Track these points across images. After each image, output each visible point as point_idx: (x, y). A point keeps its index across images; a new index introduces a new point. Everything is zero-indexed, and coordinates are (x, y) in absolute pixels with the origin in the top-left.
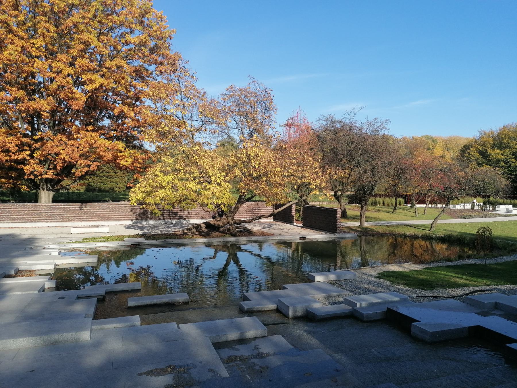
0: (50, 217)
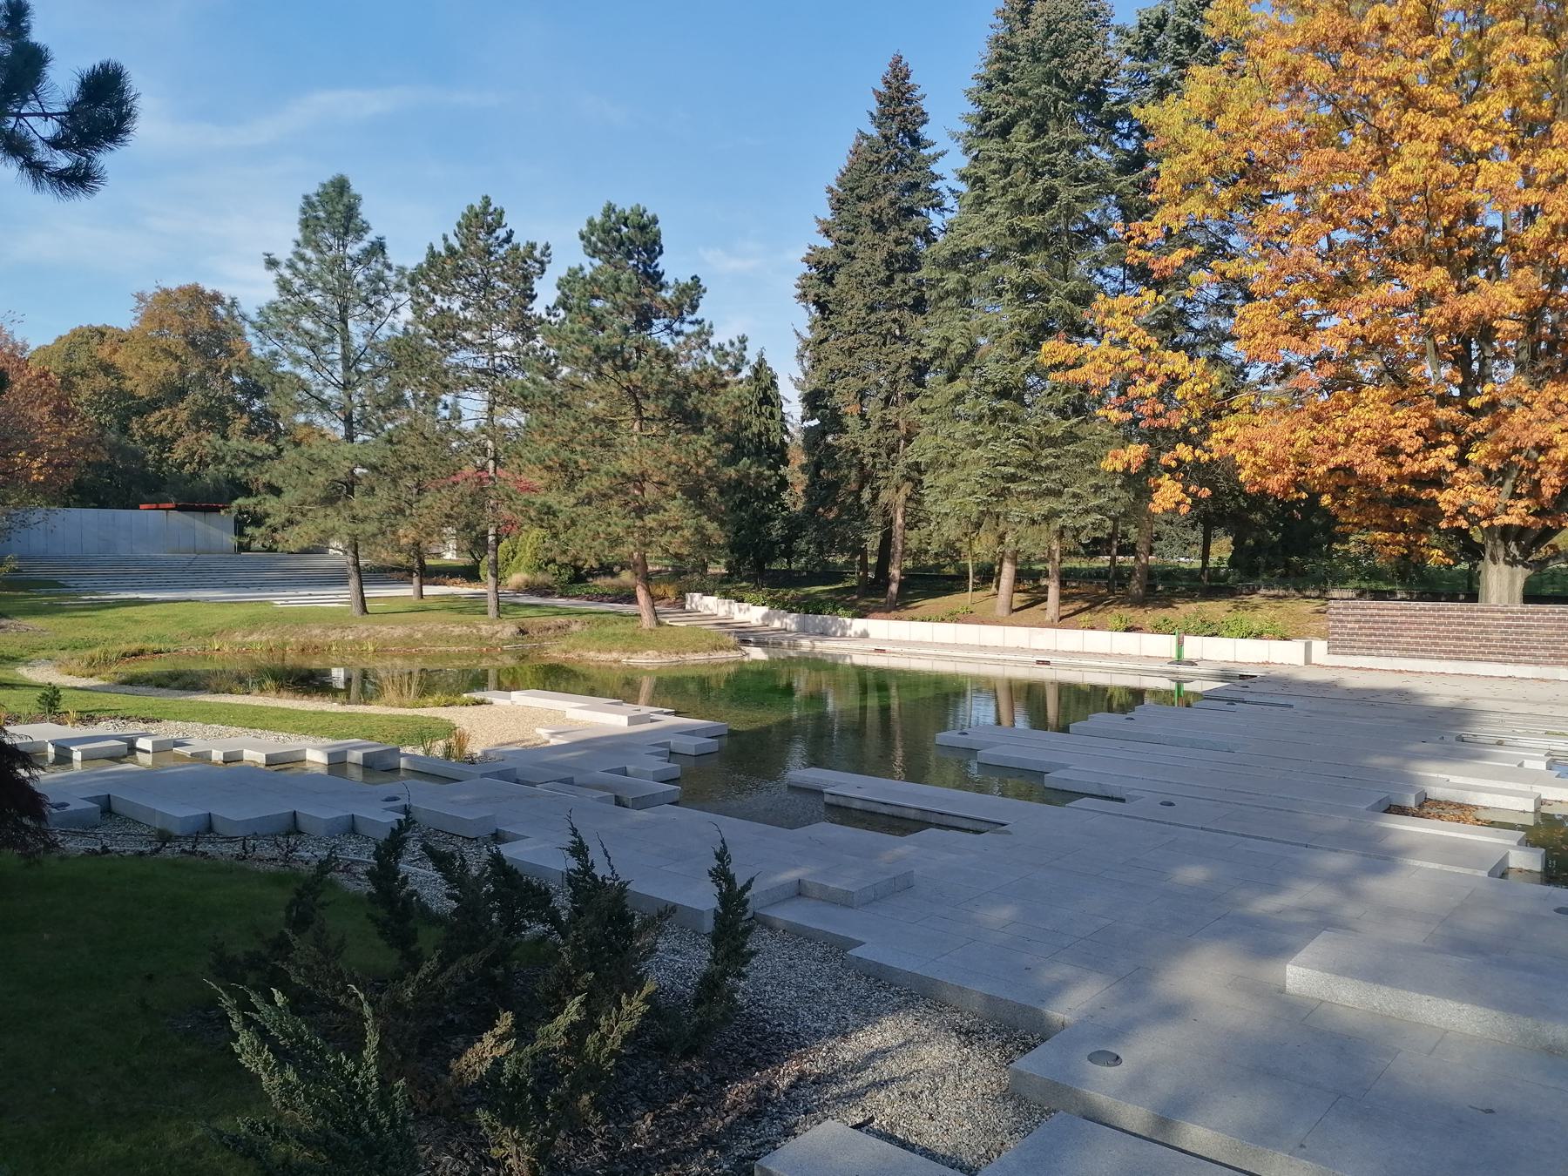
0: (1515, 648)
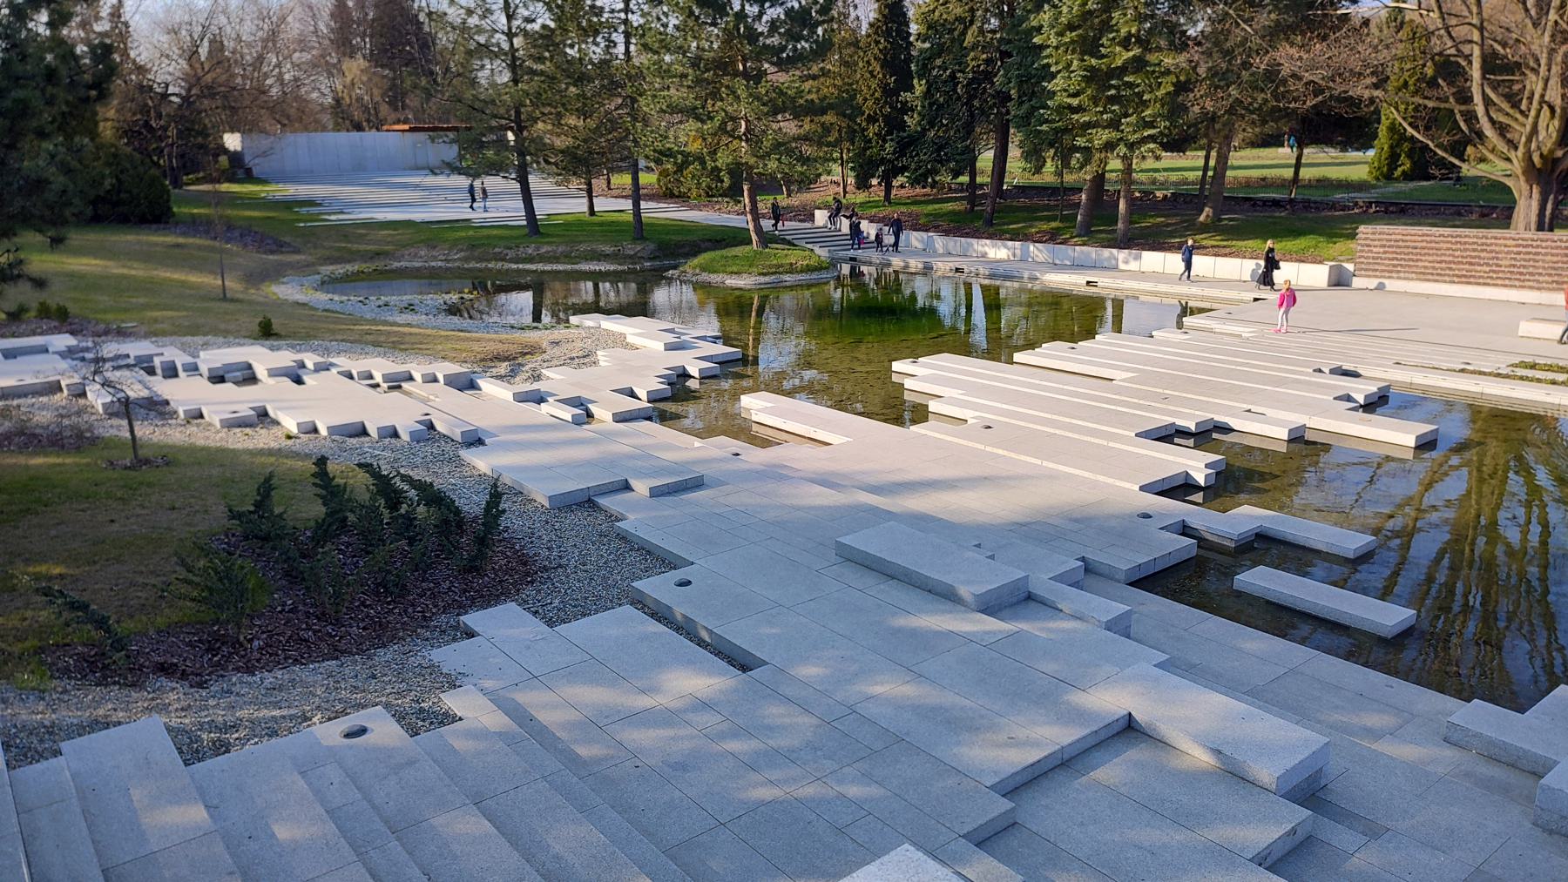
0: (1521, 274)
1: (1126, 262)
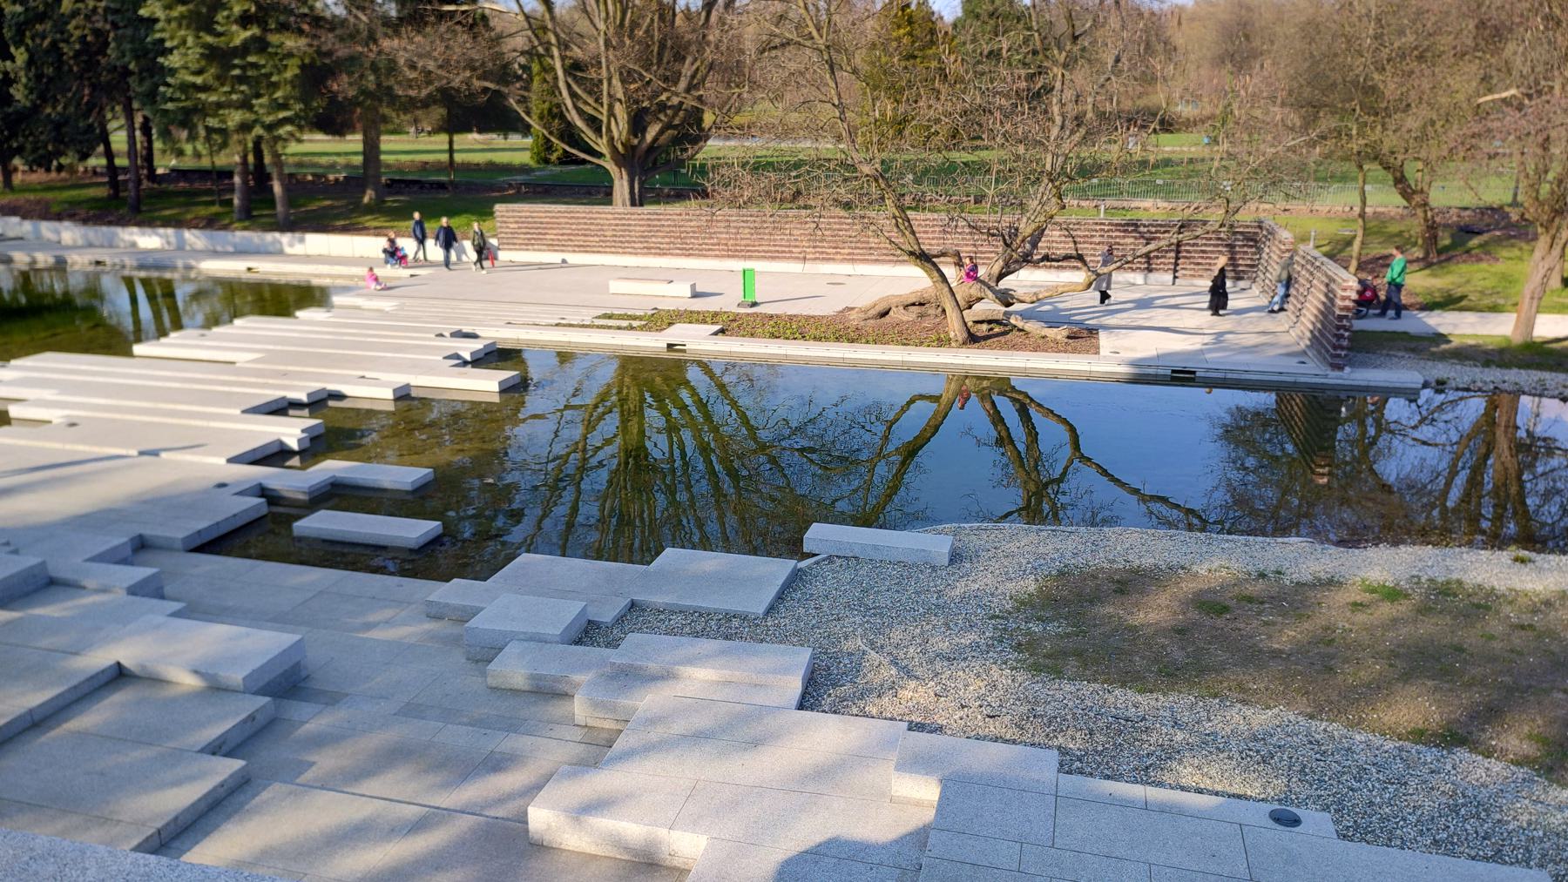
1: (291, 245)
